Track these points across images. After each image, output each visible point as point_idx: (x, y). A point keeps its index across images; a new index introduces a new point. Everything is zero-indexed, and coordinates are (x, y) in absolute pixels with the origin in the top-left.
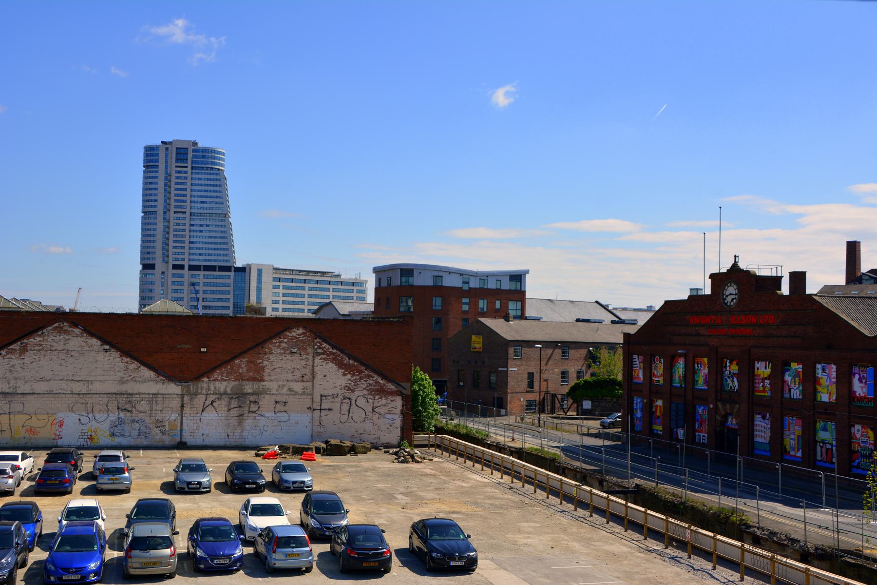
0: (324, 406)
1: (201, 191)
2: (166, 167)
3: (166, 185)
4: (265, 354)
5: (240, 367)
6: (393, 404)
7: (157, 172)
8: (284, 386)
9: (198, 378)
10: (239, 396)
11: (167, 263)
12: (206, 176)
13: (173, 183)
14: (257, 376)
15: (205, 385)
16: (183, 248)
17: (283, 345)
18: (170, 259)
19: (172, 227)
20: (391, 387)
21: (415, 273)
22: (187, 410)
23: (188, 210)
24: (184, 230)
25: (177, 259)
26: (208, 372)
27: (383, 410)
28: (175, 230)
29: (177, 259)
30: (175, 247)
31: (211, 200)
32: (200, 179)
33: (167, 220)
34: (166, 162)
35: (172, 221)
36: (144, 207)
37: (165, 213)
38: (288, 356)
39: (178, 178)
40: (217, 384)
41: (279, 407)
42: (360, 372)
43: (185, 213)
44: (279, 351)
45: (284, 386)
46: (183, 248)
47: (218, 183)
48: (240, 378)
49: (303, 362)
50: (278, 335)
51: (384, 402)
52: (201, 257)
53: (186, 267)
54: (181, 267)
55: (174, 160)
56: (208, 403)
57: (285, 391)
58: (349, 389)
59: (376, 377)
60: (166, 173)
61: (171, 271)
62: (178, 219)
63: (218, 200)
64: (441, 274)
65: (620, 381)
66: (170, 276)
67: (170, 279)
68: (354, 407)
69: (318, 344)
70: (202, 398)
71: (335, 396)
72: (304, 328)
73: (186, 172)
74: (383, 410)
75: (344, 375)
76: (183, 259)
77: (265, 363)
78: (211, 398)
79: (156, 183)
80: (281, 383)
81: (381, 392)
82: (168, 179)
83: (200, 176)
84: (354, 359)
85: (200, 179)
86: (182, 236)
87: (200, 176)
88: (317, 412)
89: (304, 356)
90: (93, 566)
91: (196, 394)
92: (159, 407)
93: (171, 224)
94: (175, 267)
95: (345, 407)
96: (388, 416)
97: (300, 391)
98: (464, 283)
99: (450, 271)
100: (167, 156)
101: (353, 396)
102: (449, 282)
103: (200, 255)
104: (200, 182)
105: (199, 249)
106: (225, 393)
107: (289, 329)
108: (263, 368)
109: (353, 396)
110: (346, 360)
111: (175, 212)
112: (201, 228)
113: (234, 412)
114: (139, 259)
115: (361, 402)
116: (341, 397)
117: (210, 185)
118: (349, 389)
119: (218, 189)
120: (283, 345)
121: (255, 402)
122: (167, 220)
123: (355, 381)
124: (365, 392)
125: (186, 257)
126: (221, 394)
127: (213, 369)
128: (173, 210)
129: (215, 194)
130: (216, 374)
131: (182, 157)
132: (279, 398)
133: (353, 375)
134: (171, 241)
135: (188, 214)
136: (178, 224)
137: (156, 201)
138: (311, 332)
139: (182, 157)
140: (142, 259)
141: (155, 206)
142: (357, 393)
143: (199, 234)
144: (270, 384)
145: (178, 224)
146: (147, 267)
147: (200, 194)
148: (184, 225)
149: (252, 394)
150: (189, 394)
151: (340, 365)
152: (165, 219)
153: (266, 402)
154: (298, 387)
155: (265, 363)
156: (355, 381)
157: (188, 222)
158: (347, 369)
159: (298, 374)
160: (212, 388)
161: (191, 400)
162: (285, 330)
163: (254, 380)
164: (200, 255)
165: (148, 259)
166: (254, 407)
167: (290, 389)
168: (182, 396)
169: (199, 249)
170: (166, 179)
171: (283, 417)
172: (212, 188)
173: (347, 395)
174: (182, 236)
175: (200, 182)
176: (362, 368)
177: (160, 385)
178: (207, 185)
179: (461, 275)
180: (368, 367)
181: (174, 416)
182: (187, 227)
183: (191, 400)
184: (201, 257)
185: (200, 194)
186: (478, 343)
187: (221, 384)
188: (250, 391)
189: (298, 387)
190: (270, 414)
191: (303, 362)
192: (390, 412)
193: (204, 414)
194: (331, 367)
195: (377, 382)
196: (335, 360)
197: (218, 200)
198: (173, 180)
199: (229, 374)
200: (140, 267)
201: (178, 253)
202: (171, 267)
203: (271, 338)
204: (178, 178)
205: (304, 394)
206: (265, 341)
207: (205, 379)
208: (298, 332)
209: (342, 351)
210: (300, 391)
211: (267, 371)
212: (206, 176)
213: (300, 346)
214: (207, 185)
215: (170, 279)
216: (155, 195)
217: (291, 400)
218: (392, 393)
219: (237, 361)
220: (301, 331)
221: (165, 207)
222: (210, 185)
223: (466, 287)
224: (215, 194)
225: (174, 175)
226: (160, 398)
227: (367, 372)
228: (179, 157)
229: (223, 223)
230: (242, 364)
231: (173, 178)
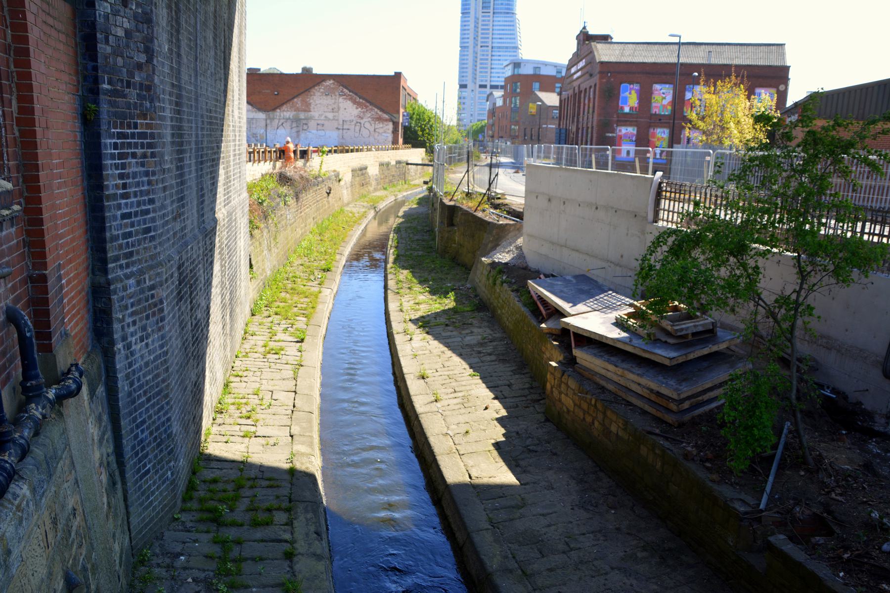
0: (345, 127)
1: (500, 30)
2: (475, 14)
3: (475, 27)
4: (311, 95)
5: (297, 103)
6: (387, 127)
7: (469, 17)
8: (322, 115)
9: (274, 109)
10: (297, 120)
11: (475, 83)
12: (504, 19)
13: (480, 25)
14: (307, 108)
15: (278, 114)
16: (486, 72)
17: (322, 90)
18: (478, 80)
19: (479, 57)
20: (386, 116)
21: (522, 65)
22: (269, 127)
23: (490, 44)
24: (487, 60)
25: (482, 81)
26: (279, 106)
27: (381, 131)
28: (481, 59)
29: (482, 81)
30: (481, 72)
31: (507, 36)
32: (499, 21)
33: (475, 53)
34: (476, 9)
35: (479, 53)
36: (461, 43)
37: (474, 47)
38: (325, 97)
39: (483, 21)
40: (285, 113)
41: (320, 127)
42: (366, 107)
43: (488, 46)
44: (319, 94)
45: (322, 115)
46: (486, 72)
47: (512, 23)
48: (297, 110)
49: (333, 101)
50: (318, 84)
51: (381, 125)
52: (498, 79)
53: (488, 86)
54: (485, 86)
55: (481, 8)
56: (280, 124)
57: (323, 118)
58: (360, 117)
59: (376, 110)
60: (476, 17)
61: (478, 89)
62: (483, 51)
63: (512, 36)
64: (539, 66)
65: (613, 131)
66: (477, 92)
67: (478, 95)
68: (363, 129)
69: (832, 198)
70: (276, 121)
71: (351, 121)
72: (334, 80)
73: (489, 16)
74: (381, 131)
75: (357, 108)
76: (486, 81)
77: (311, 101)
78: (282, 121)
79: (469, 25)
80: (320, 113)
81: (380, 119)
82: (476, 22)
83: (499, 19)
84: (364, 99)
85: (499, 21)
86: (486, 64)
87: (499, 19)
88: (341, 131)
89: (334, 97)
90: (431, 283)
91: (274, 119)
92: (254, 126)
93: (479, 55)
94: (481, 86)
95: (357, 128)
96: (384, 134)
97: (331, 118)
98: (557, 72)
99: (546, 64)
100: (476, 4)
101: (362, 121)
102: (544, 71)
103: (499, 77)
104: (499, 23)
105: (498, 73)
106: (289, 118)
107: (324, 80)
108: (310, 104)
109: (362, 121)
110: (358, 99)
111: (481, 47)
112: (499, 58)
113: (295, 130)
114: (457, 81)
115: (367, 125)
116: (355, 122)
117: (506, 26)
118: (360, 117)
119: (511, 28)
120: (322, 90)
121: (306, 124)
122: (475, 53)
123: (364, 112)
124: (370, 119)
125: (488, 79)
126: (287, 119)
127: (282, 104)
128: (480, 44)
129: (509, 32)
130: (284, 107)
131: (487, 5)
132: (319, 122)
133: (362, 109)
134: (478, 68)
135: (490, 47)
136: (483, 55)
137: (468, 38)
138: (338, 82)
139: (487, 5)
140: (460, 80)
141: (467, 43)
142: (365, 120)
143: (497, 62)
144: (315, 113)
145: (483, 55)
146: (463, 86)
147: (499, 32)
148: (487, 55)
149: (304, 119)
150: (270, 118)
151: (354, 102)
152: (474, 52)
153: (312, 124)
154: (330, 116)
155: (311, 101)
156: (364, 112)
157: (490, 53)
158: (359, 105)
159: (330, 107)
160: (282, 115)
161: (271, 122)
162: (322, 81)
163: (305, 111)
164: (499, 77)
165: (463, 81)
166: (305, 127)
167: (326, 117)
168: (266, 120)
169: (498, 73)
170: (475, 22)
171: (322, 133)
172: (507, 28)
173: (359, 121)
174: (486, 64)
175: (499, 23)
176: (368, 104)
177: (254, 113)
178: (504, 26)
179: (555, 66)
180: (371, 104)
181: (262, 131)
182: (489, 57)
183: (271, 122)
184: (498, 79)
185: (499, 32)
186: (531, 108)
187: (286, 113)
188: (303, 117)
189: (330, 116)
190: (314, 131)
191: (333, 101)
192: (385, 132)
193: (278, 130)
194: (349, 104)
195: (377, 113)
196: (351, 99)
197: (512, 36)
198: (480, 23)
199: (291, 107)
200: (458, 86)
201: (483, 77)
202: (478, 86)
203: (314, 86)
204: (483, 21)
205: (334, 119)
206: (311, 88)
207: (278, 110)
208: (330, 82)
209: (356, 94)
210: (331, 118)
211: (312, 106)
212: (504, 19)
213: (328, 93)
214: (504, 26)
215: (478, 95)
216: (468, 34)
217: (326, 123)
218: (386, 120)
219: (295, 100)
220: (332, 82)
221: (474, 43)
222: (506, 26)
223: (559, 76)
224: (509, 32)
225: (481, 19)
226: (254, 121)
227: (370, 107)
228: (485, 5)
229: (515, 54)
230: (298, 101)
231: (480, 20)
